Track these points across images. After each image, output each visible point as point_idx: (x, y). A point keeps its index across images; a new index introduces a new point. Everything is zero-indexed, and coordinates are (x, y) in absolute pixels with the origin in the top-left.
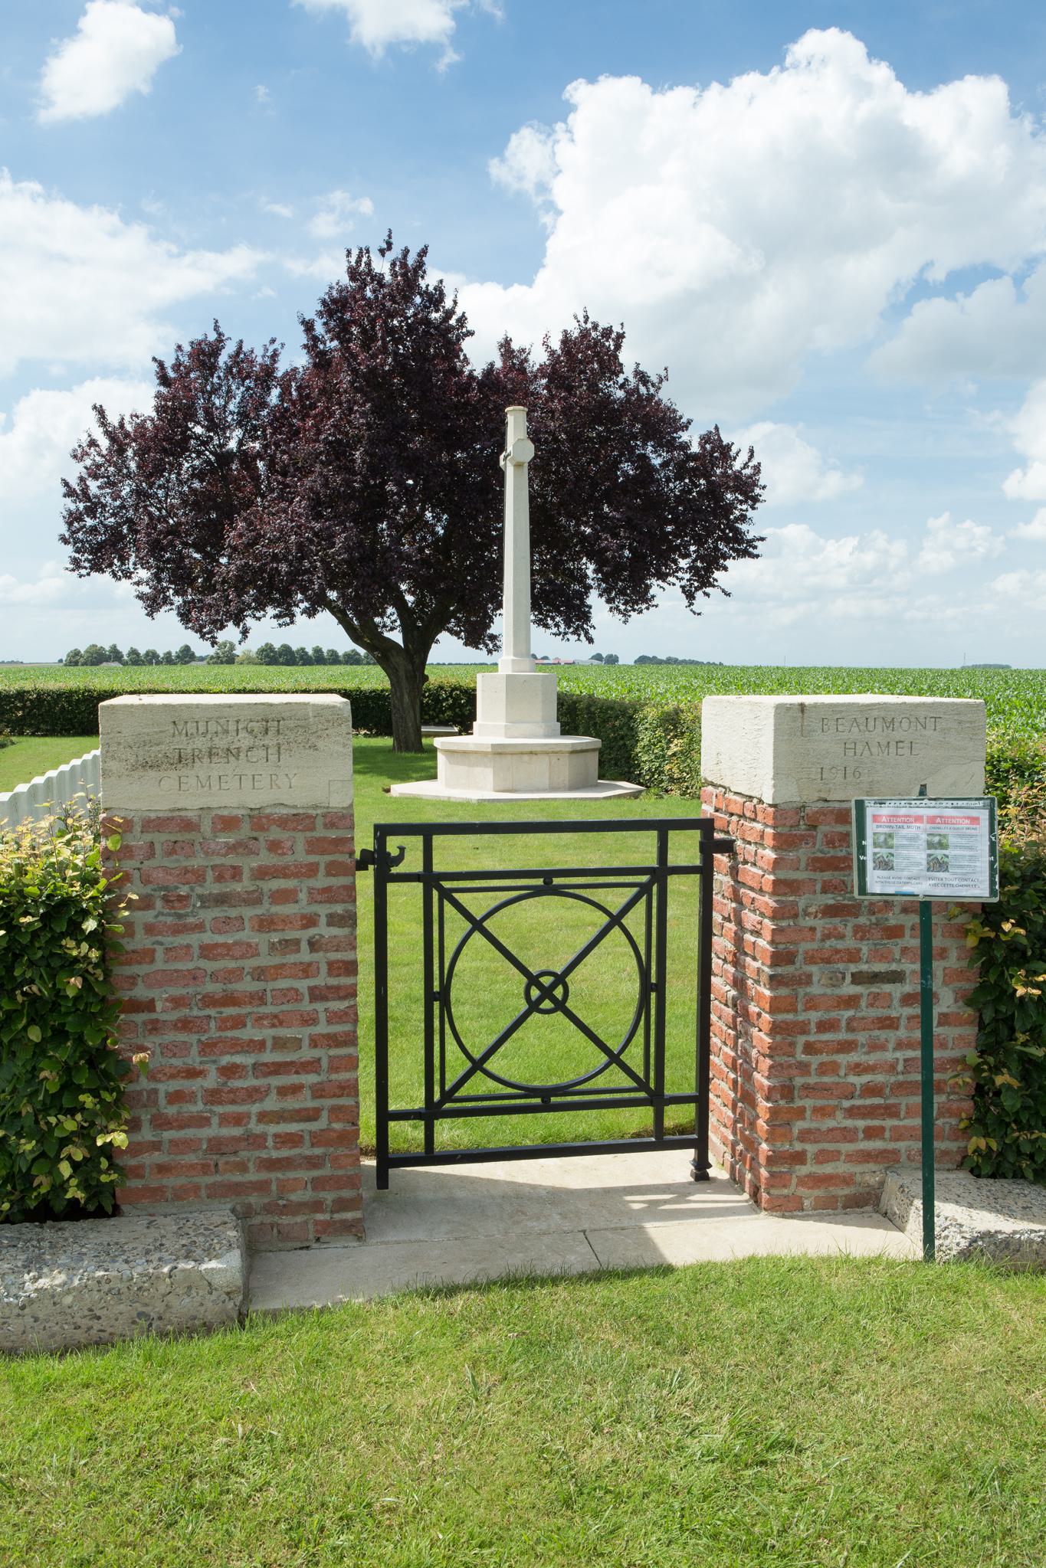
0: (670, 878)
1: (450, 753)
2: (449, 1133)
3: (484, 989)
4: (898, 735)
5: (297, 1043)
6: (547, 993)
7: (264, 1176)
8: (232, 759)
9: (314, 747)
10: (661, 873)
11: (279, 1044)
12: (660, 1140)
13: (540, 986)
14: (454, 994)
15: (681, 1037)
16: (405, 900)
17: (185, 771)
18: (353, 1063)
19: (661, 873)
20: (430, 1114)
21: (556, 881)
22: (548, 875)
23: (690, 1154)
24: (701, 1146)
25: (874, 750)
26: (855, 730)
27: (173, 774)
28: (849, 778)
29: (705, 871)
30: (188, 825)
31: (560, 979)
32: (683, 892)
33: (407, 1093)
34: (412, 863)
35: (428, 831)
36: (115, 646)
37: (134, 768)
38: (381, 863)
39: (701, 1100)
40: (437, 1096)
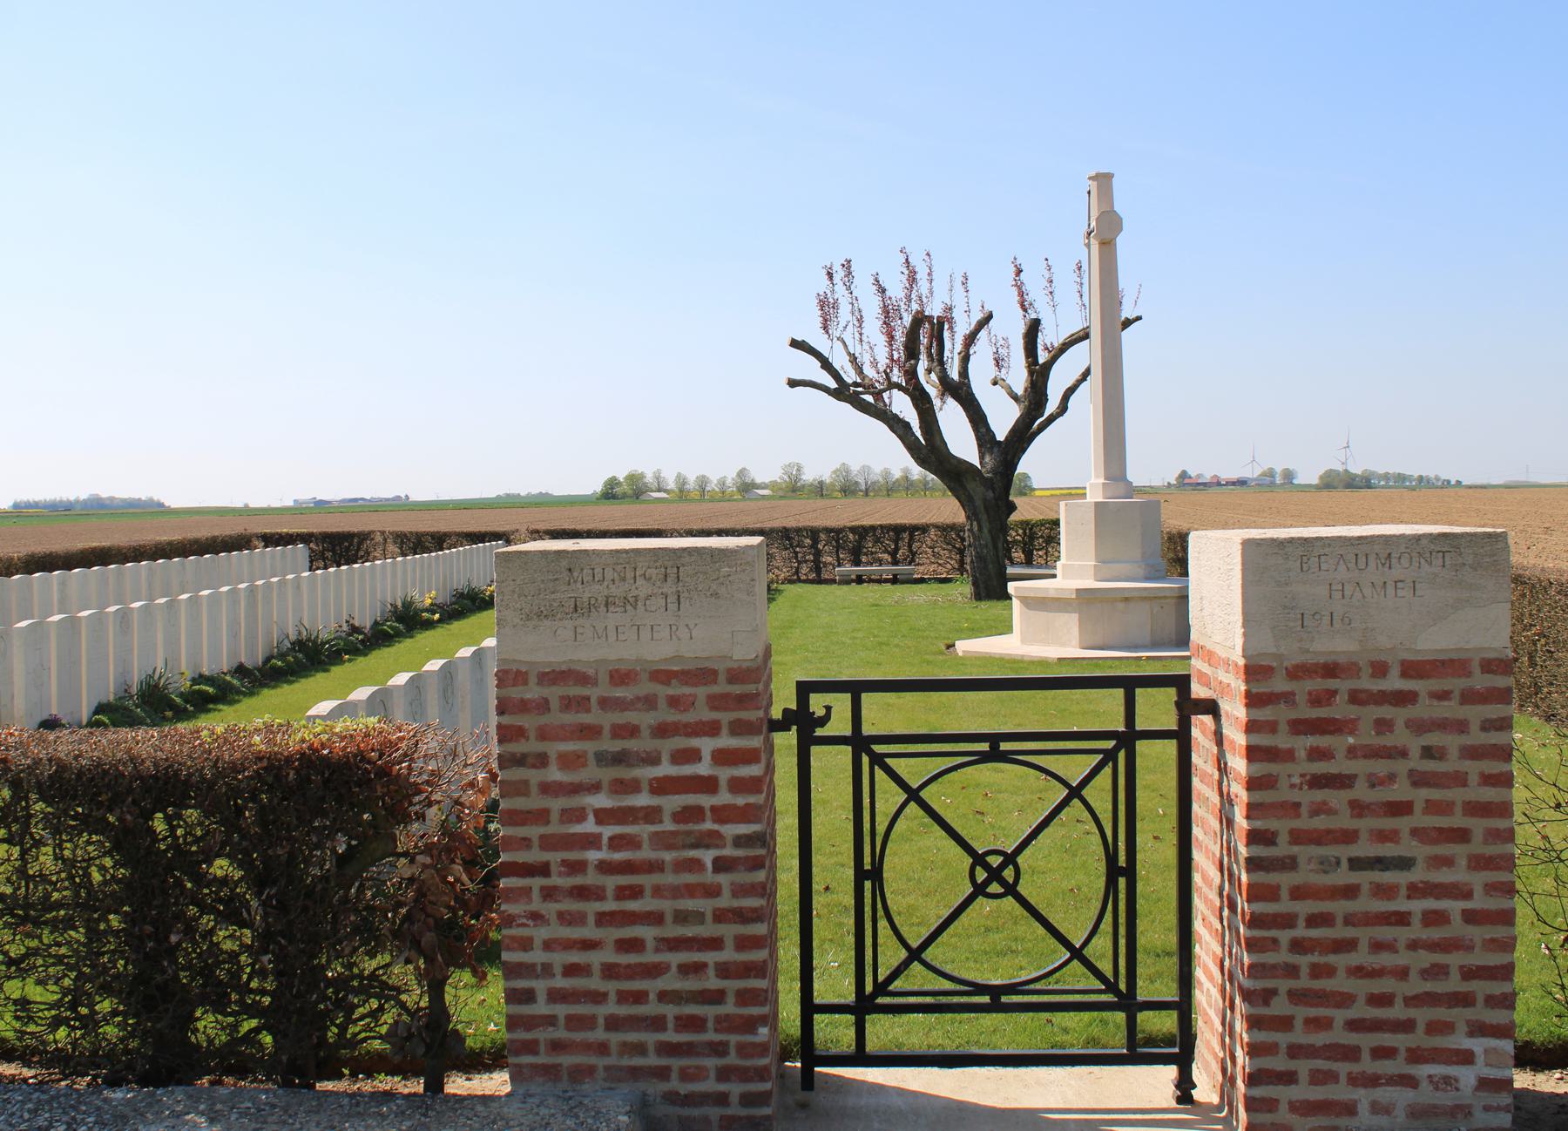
0: (1138, 743)
1: (1028, 602)
2: (883, 1031)
3: (923, 873)
4: (1397, 573)
5: (699, 917)
6: (995, 874)
7: (663, 1062)
8: (629, 607)
9: (716, 595)
10: (1128, 738)
11: (682, 917)
12: (1137, 1053)
13: (1003, 866)
14: (887, 874)
15: (1156, 931)
16: (831, 765)
17: (580, 621)
18: (769, 941)
19: (1128, 738)
20: (862, 1007)
21: (1004, 746)
22: (995, 739)
23: (1171, 1071)
24: (1184, 1061)
25: (1368, 591)
26: (1342, 567)
27: (569, 624)
28: (1337, 625)
29: (1182, 737)
30: (583, 679)
31: (1010, 859)
32: (1156, 758)
33: (836, 983)
34: (840, 725)
35: (855, 689)
36: (659, 471)
37: (528, 618)
38: (804, 723)
39: (1184, 1006)
40: (869, 988)
